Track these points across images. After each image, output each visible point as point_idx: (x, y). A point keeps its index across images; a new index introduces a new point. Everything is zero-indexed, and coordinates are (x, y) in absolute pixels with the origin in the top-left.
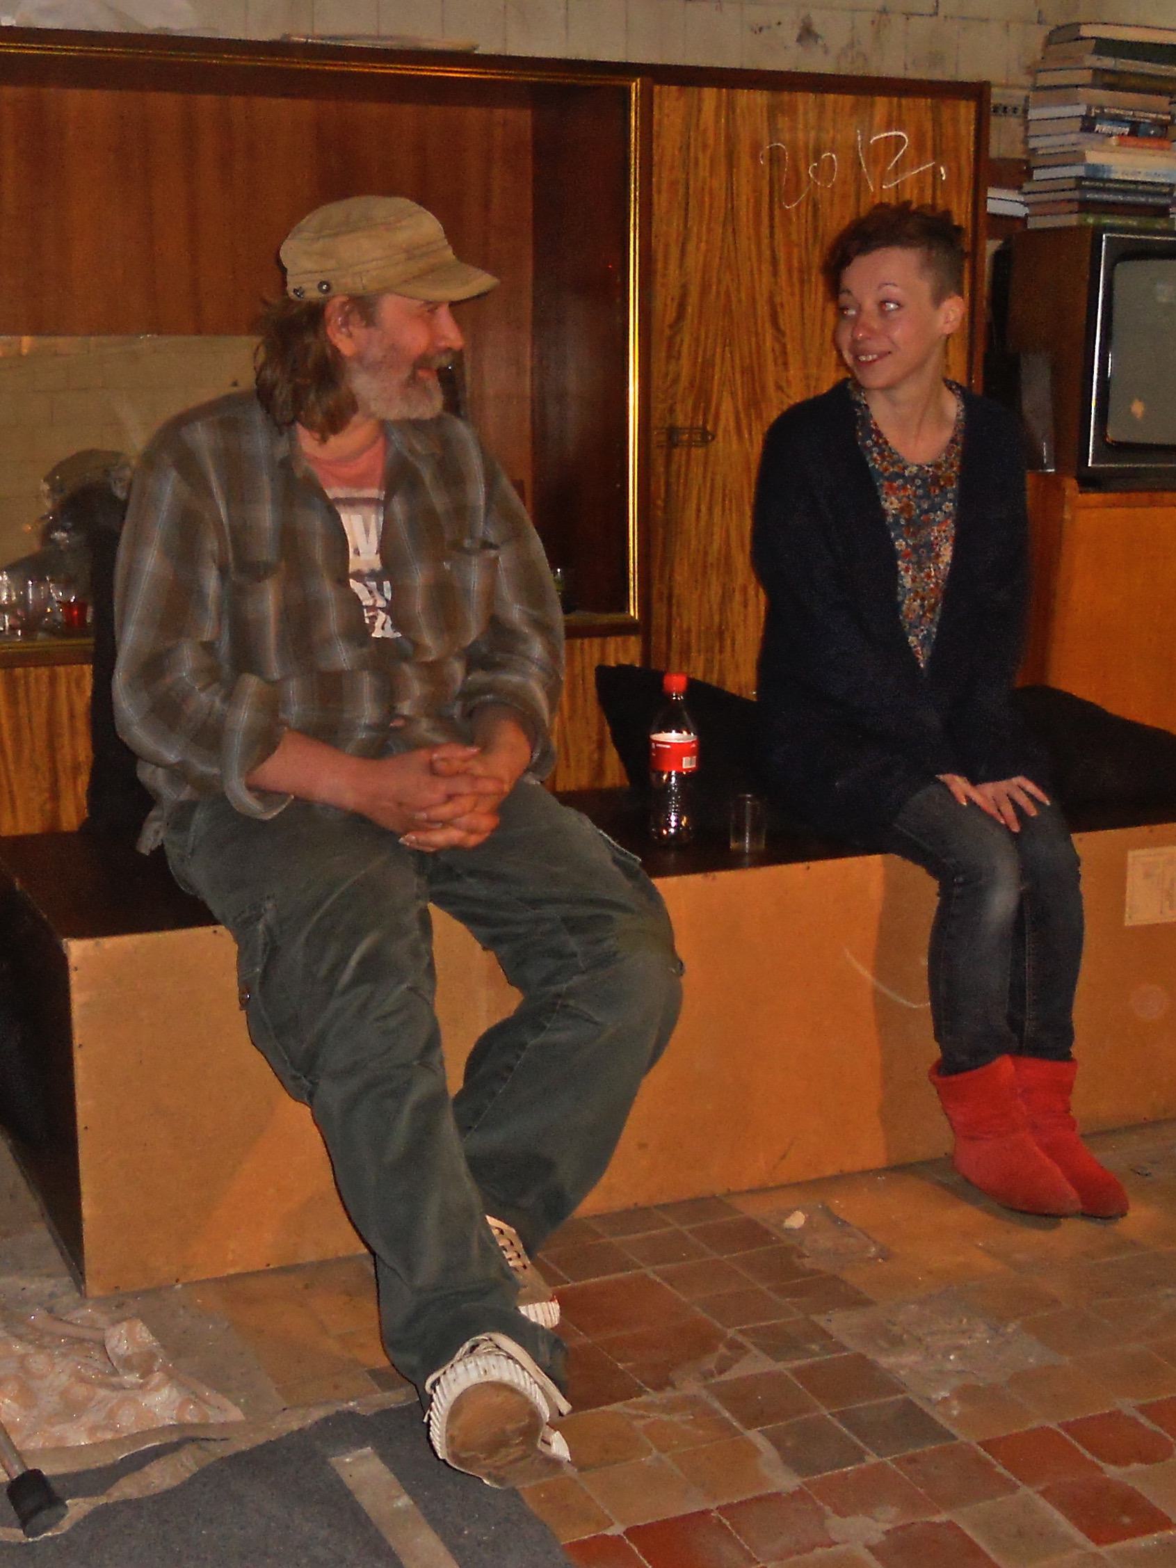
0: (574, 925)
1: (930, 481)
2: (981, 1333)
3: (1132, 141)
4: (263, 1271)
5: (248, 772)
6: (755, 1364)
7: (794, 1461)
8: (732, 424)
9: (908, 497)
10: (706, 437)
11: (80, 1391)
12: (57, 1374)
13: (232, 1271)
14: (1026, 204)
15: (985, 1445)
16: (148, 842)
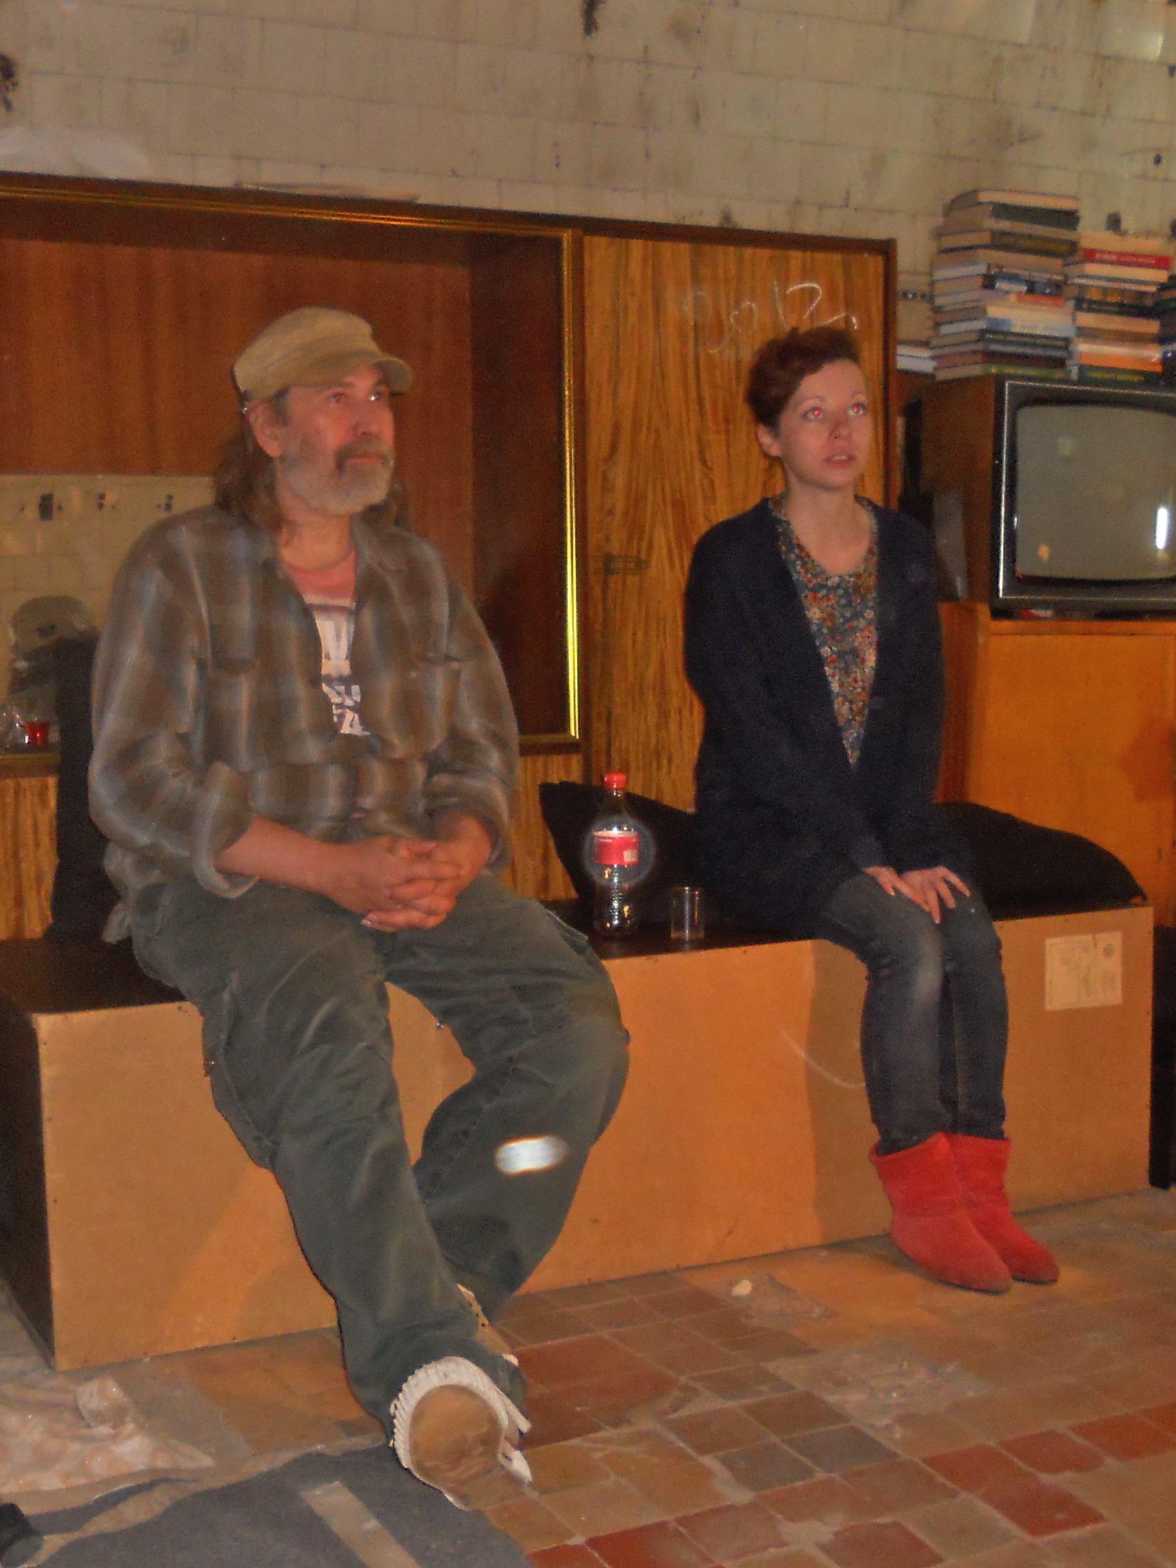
0: (522, 992)
1: (851, 591)
2: (922, 1375)
3: (1030, 297)
4: (227, 1346)
5: (218, 852)
6: (708, 1403)
7: (744, 1478)
8: (665, 552)
9: (832, 606)
10: (641, 565)
11: (53, 1445)
12: (30, 1431)
13: (199, 1345)
14: (933, 358)
15: (930, 1461)
16: (112, 934)
